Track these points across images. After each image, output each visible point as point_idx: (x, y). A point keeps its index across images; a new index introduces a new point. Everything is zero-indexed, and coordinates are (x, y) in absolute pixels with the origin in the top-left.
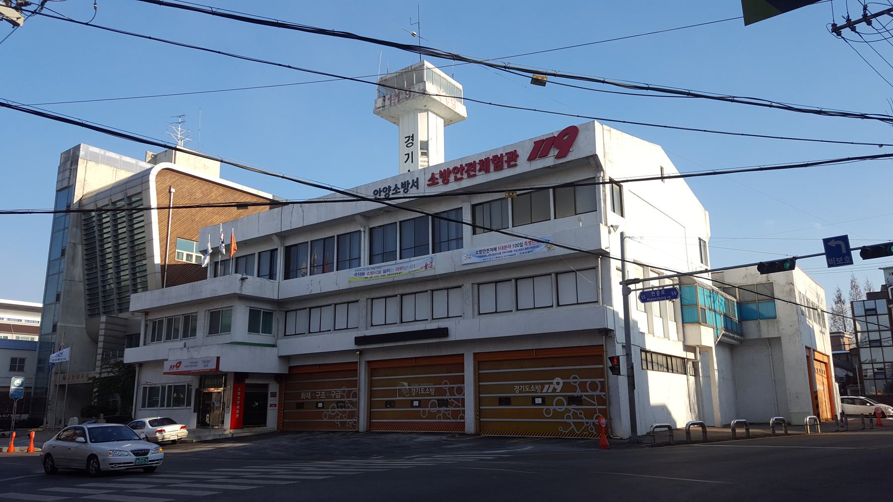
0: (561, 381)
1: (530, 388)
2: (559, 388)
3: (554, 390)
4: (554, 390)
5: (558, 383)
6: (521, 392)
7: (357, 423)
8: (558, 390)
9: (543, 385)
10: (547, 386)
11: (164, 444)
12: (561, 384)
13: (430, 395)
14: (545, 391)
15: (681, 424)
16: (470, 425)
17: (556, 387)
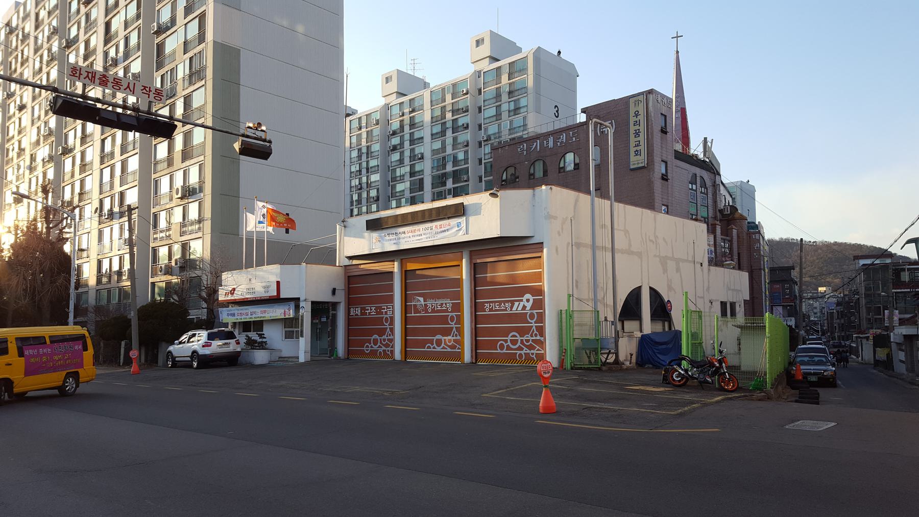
0: (531, 298)
1: (500, 305)
2: (529, 305)
3: (524, 307)
4: (524, 307)
5: (528, 301)
6: (491, 310)
7: (392, 352)
8: (528, 308)
9: (513, 303)
10: (516, 304)
11: (138, 17)
12: (531, 301)
13: (446, 311)
14: (514, 309)
15: (302, 359)
16: (398, 356)
17: (526, 304)
